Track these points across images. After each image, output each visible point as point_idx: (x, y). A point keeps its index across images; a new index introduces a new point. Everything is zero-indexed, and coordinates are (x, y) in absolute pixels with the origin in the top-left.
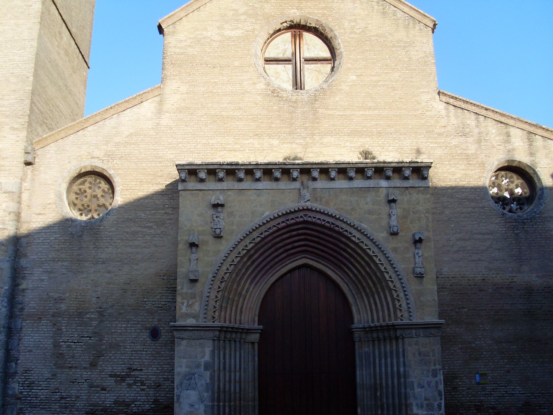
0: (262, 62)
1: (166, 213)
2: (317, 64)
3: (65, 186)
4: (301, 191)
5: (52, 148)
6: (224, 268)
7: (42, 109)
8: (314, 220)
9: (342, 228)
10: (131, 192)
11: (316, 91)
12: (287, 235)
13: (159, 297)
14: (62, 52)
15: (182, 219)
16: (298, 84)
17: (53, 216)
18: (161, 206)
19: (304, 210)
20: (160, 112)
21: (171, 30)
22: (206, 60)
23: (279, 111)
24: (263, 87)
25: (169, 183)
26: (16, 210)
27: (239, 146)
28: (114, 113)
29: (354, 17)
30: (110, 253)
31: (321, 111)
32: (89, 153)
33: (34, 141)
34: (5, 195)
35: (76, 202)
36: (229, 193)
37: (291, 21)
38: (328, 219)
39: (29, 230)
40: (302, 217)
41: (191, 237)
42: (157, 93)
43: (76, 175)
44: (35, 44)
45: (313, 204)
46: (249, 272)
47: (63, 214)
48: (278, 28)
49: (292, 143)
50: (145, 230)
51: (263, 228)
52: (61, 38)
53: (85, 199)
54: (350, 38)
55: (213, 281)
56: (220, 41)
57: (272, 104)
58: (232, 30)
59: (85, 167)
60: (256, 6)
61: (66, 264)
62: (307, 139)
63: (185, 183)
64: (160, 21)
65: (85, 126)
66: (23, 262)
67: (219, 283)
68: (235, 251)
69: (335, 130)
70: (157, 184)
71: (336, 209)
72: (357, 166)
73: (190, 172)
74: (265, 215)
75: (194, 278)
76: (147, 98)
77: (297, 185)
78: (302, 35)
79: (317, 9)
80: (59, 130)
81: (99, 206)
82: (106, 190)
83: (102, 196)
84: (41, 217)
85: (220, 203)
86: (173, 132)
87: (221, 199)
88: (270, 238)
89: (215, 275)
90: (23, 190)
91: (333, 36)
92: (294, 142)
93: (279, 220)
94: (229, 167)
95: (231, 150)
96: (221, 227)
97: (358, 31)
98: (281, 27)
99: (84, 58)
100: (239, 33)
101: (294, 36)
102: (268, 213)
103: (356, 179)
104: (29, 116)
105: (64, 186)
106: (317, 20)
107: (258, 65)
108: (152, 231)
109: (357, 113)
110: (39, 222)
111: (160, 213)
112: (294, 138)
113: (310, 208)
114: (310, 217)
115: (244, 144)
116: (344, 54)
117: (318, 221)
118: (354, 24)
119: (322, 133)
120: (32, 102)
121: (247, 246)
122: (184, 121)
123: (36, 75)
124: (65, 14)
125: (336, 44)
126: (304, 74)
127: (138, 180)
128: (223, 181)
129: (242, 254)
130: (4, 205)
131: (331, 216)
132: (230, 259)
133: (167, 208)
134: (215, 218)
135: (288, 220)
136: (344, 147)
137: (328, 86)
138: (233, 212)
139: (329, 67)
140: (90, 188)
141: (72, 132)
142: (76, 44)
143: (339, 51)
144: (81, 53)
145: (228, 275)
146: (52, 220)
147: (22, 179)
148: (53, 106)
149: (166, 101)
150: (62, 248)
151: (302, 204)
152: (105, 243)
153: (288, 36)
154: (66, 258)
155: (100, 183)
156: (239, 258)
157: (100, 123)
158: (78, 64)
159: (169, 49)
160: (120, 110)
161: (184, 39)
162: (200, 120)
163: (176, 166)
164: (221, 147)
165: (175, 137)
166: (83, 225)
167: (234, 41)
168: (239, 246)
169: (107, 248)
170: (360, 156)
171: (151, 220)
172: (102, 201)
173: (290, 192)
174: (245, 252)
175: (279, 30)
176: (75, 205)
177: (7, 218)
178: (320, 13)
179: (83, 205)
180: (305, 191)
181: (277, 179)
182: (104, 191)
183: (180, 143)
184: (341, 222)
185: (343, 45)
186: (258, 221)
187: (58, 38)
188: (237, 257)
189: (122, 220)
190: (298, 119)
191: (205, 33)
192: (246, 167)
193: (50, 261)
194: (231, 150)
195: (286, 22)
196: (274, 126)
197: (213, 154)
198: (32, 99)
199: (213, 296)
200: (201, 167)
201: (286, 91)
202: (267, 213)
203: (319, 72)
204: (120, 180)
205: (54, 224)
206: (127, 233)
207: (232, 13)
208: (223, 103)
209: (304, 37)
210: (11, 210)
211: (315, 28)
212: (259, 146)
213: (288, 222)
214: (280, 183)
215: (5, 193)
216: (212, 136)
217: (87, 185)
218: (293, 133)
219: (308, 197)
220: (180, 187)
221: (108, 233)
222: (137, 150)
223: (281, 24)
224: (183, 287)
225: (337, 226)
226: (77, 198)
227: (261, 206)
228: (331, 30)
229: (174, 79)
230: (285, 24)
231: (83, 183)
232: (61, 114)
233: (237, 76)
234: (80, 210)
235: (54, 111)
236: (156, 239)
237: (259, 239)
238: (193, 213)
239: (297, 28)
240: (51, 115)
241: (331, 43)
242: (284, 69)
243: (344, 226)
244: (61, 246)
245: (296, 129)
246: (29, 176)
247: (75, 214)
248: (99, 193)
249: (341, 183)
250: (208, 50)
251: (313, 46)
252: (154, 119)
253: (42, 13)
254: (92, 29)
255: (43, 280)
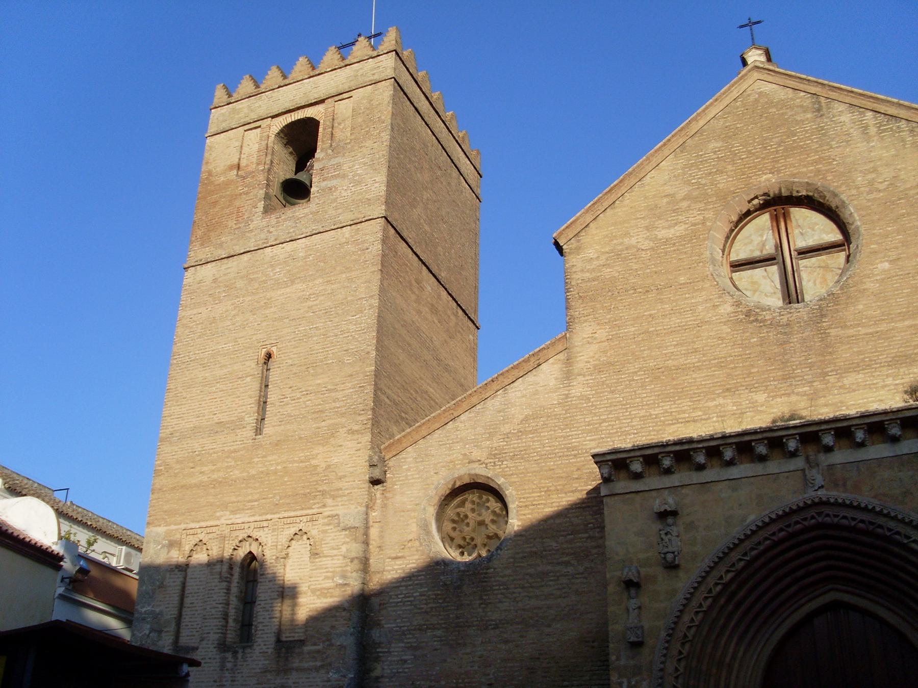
0: (726, 269)
1: (590, 537)
2: (821, 255)
3: (431, 511)
4: (807, 472)
5: (410, 454)
6: (686, 618)
7: (395, 397)
8: (836, 520)
9: (889, 530)
10: (533, 509)
11: (821, 300)
12: (792, 553)
13: (587, 678)
14: (425, 310)
15: (610, 542)
16: (791, 294)
17: (416, 560)
18: (582, 527)
19: (814, 504)
20: (568, 376)
21: (573, 246)
22: (634, 283)
23: (761, 345)
24: (730, 309)
25: (591, 487)
26: (361, 554)
27: (700, 413)
28: (498, 387)
29: (872, 165)
30: (505, 610)
31: (833, 332)
32: (465, 455)
33: (382, 447)
34: (344, 533)
35: (453, 534)
36: (685, 491)
37: (765, 194)
38: (860, 516)
39: (383, 584)
40: (813, 517)
41: (626, 570)
42: (560, 348)
43: (448, 492)
44: (375, 302)
45: (829, 493)
46: (733, 623)
47: (431, 555)
48: (744, 211)
49: (789, 395)
50: (558, 568)
51: (748, 544)
52: (422, 288)
53: (466, 529)
54: (869, 200)
55: (667, 642)
56: (652, 248)
57: (748, 334)
58: (669, 227)
59: (460, 478)
60: (703, 182)
61: (439, 633)
62: (815, 384)
63: (612, 484)
64: (554, 235)
65: (456, 414)
66: (375, 634)
67: (678, 646)
68: (703, 588)
69: (863, 360)
70: (572, 492)
71: (875, 497)
72: (900, 415)
73: (615, 464)
74: (748, 521)
75: (636, 639)
76: (547, 357)
77: (799, 463)
78: (789, 213)
79: (805, 166)
80: (417, 425)
81: (489, 537)
82: (497, 510)
83: (493, 521)
84: (399, 562)
85: (669, 509)
86: (592, 406)
87: (671, 502)
88: (762, 560)
89: (671, 632)
90: (371, 523)
91: (839, 204)
92: (793, 392)
93: (774, 528)
94: (678, 448)
95: (688, 422)
96: (674, 549)
97: (882, 187)
98: (750, 207)
99: (467, 314)
100: (680, 230)
101: (775, 219)
102: (753, 517)
103: (906, 439)
104: (373, 409)
105: (431, 512)
106: (807, 183)
107: (719, 275)
108: (570, 569)
109: (899, 325)
110: (396, 570)
111: (581, 538)
112: (791, 385)
113: (824, 499)
114: (828, 515)
115: (709, 408)
116: (862, 230)
117: (845, 522)
118: (873, 175)
119: (840, 369)
120: (377, 388)
121: (721, 578)
122: (607, 385)
123: (380, 347)
124: (424, 252)
125: (847, 216)
126: (799, 276)
127: (543, 487)
128: (673, 473)
129: (714, 593)
130: (344, 548)
131: (865, 509)
132: (694, 603)
133: (591, 529)
134: (663, 536)
135: (789, 526)
136: (884, 387)
137: (842, 289)
138: (693, 522)
139: (842, 256)
140: (473, 510)
141: (437, 425)
142: (450, 294)
143: (853, 227)
144: (461, 308)
145: (693, 631)
146: (414, 565)
147: (367, 507)
148: (417, 392)
149: (576, 357)
150: (432, 608)
151: (811, 495)
152: (497, 594)
153: (765, 219)
154: (438, 624)
155: (488, 500)
156: (710, 600)
157: (479, 407)
158: (457, 324)
159: (574, 276)
160: (507, 382)
161: (596, 255)
162: (633, 380)
163: (594, 456)
164: (671, 418)
165: (595, 414)
166: (462, 568)
167: (674, 244)
168: (709, 579)
169: (500, 602)
170: (906, 397)
171: (567, 551)
172: (492, 528)
173: (787, 477)
174: (719, 588)
175: (748, 213)
176: (452, 539)
177: (349, 568)
178: (811, 171)
179: (464, 539)
180: (814, 471)
181: (762, 459)
182: (494, 512)
183: (604, 421)
184: (885, 519)
185: (859, 216)
186: (737, 532)
187: (415, 290)
188: (706, 598)
189: (521, 555)
190: (795, 353)
191: (626, 240)
192: (706, 444)
193: (414, 630)
194: (688, 422)
195: (756, 197)
196: (756, 370)
197: (658, 431)
198: (376, 384)
199: (670, 668)
200: (632, 454)
201: (769, 309)
202: (752, 517)
203: (826, 268)
204: (514, 493)
205: (419, 571)
206: (531, 575)
207: (665, 200)
208: (667, 347)
209: (792, 216)
210: (354, 555)
211: (807, 197)
212: (735, 408)
213: (790, 530)
214: (769, 463)
215: (345, 529)
216: (654, 403)
217: (468, 505)
218: (789, 378)
219: (819, 480)
220: (603, 492)
221: (500, 579)
222: (538, 441)
223: (749, 202)
224: (619, 658)
225: (880, 526)
226: (454, 529)
227: (735, 507)
228: (835, 195)
229: (586, 321)
230: (756, 202)
231: (462, 504)
232: (433, 404)
233: (686, 298)
234: (460, 546)
235: (419, 399)
236: (578, 581)
237: (742, 564)
238: (629, 534)
239: (778, 204)
240: (414, 406)
241: (838, 216)
242: (765, 274)
243: (892, 524)
244: (430, 605)
245: (794, 370)
246: (378, 501)
247: (453, 554)
248: (487, 517)
249: (879, 450)
250: (635, 267)
251: (809, 227)
252: (560, 388)
253: (384, 256)
254: (477, 269)
255: (405, 661)
